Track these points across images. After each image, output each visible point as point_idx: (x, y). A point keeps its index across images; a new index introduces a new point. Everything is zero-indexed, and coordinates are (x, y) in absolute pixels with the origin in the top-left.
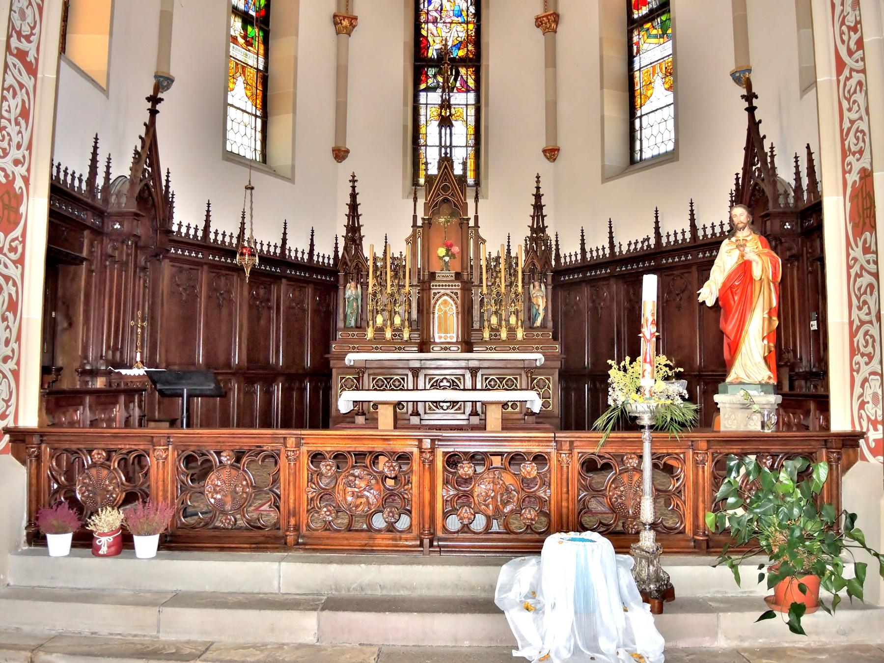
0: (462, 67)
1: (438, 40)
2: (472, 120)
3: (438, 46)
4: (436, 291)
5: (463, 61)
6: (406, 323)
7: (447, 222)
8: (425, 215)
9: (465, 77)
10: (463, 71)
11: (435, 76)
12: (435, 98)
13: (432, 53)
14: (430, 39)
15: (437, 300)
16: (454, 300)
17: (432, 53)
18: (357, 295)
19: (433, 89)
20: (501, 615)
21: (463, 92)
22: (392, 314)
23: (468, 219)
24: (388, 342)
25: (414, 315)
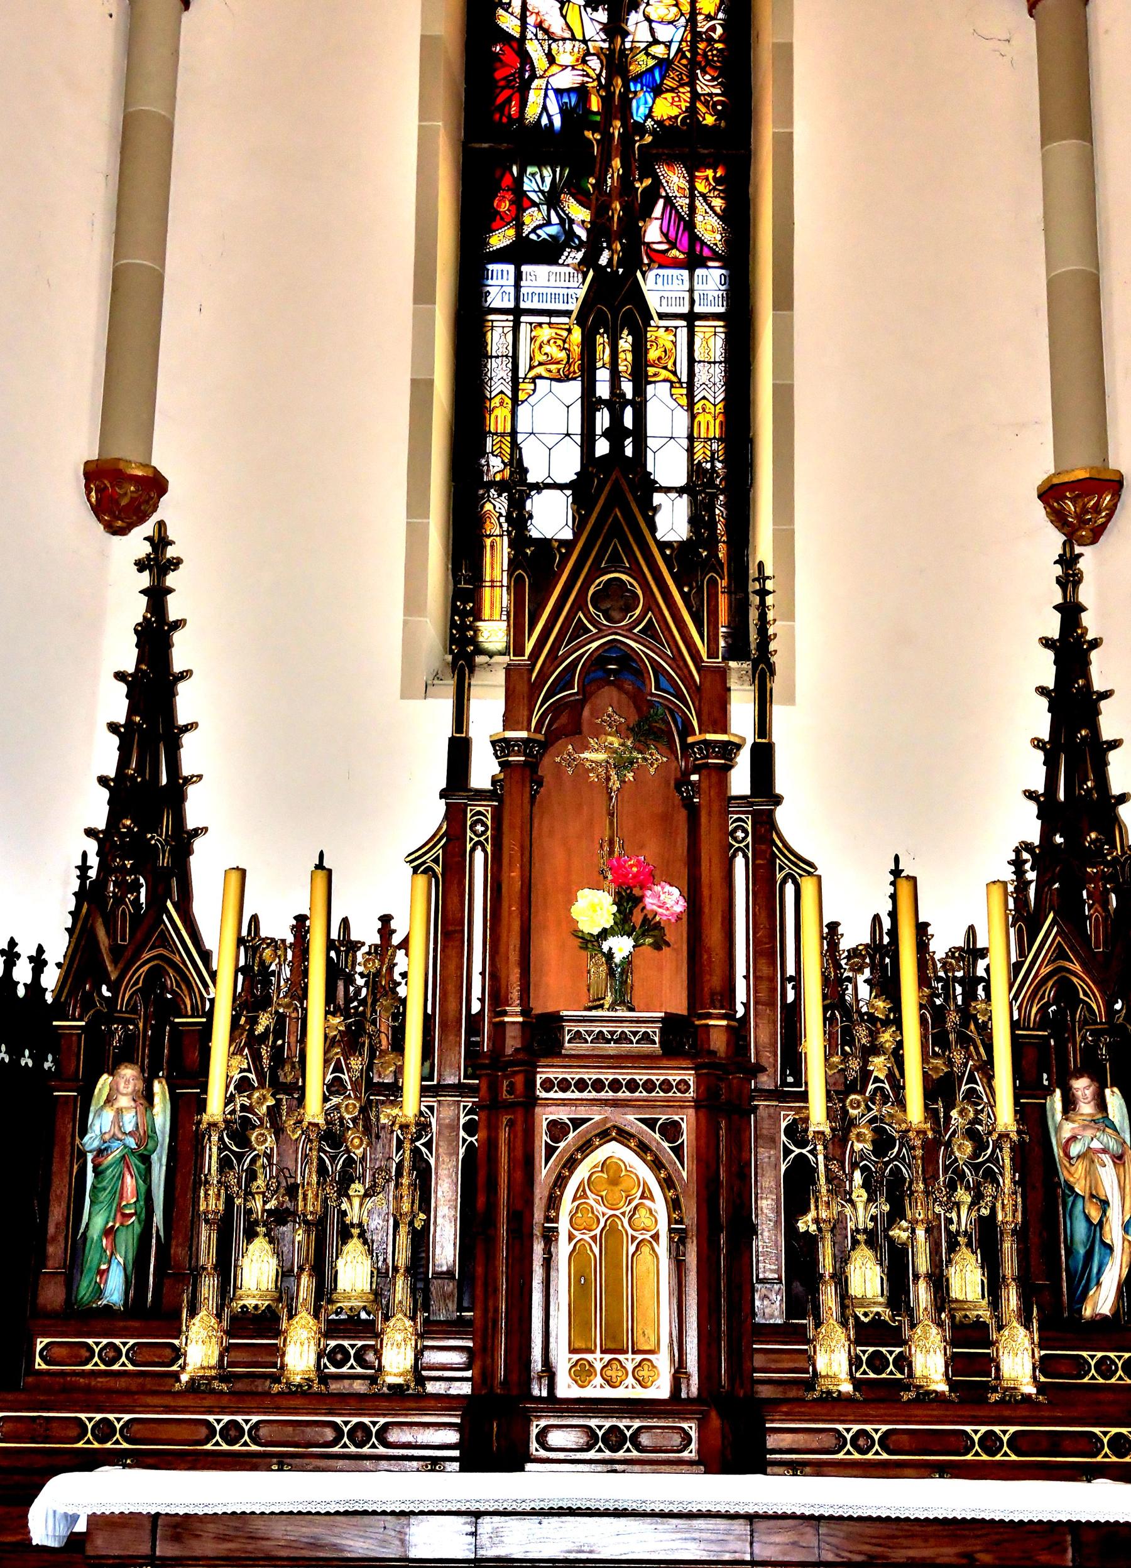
0: (670, 161)
1: (566, 54)
2: (711, 379)
3: (566, 80)
4: (563, 1115)
5: (681, 143)
6: (401, 1290)
7: (622, 764)
8: (509, 721)
9: (683, 202)
10: (674, 180)
11: (552, 199)
12: (557, 285)
13: (541, 106)
14: (534, 49)
15: (571, 1164)
16: (657, 1165)
17: (541, 106)
18: (146, 1135)
19: (547, 253)
20: (181, 6)
21: (676, 264)
22: (329, 1233)
23: (729, 750)
24: (302, 1396)
25: (445, 1250)
